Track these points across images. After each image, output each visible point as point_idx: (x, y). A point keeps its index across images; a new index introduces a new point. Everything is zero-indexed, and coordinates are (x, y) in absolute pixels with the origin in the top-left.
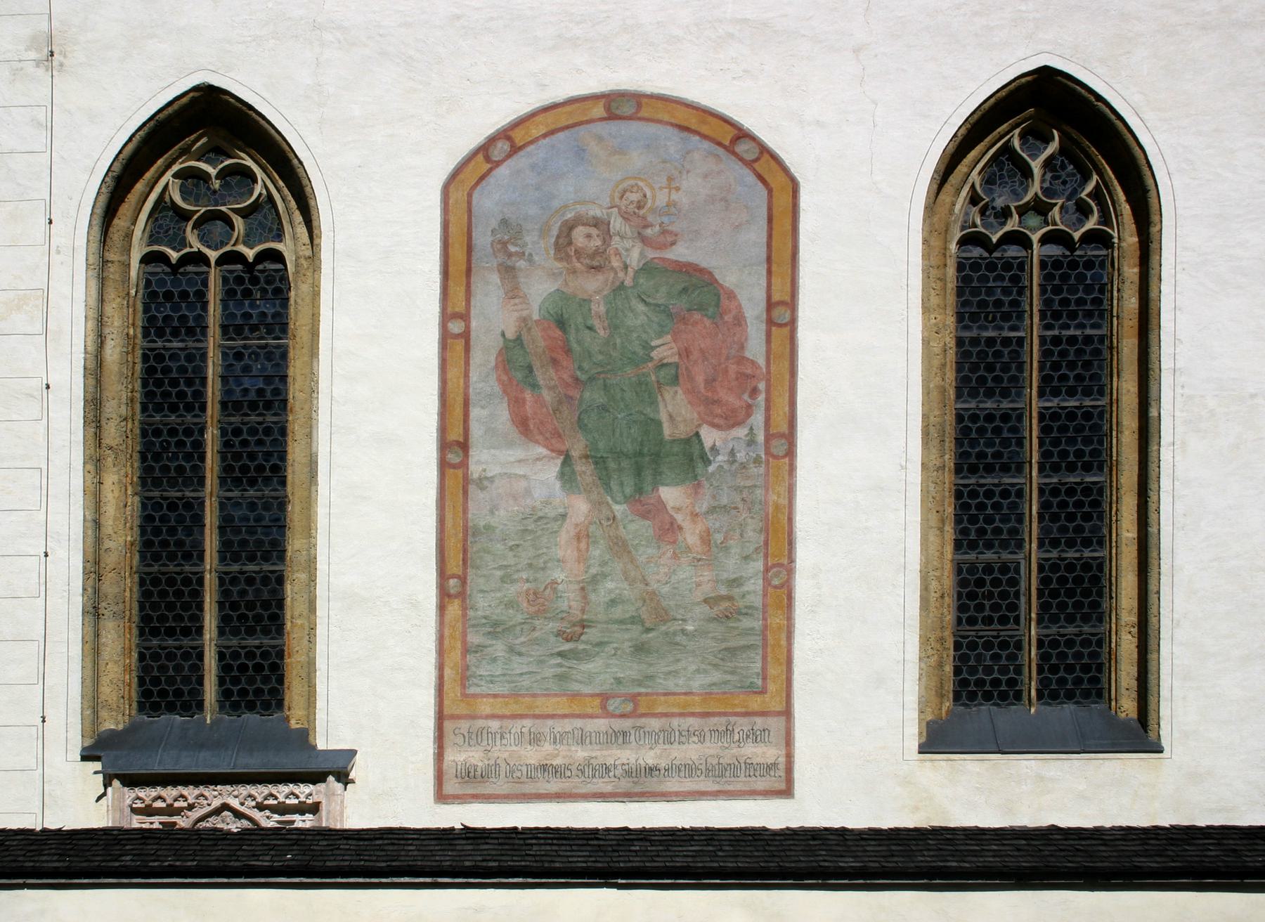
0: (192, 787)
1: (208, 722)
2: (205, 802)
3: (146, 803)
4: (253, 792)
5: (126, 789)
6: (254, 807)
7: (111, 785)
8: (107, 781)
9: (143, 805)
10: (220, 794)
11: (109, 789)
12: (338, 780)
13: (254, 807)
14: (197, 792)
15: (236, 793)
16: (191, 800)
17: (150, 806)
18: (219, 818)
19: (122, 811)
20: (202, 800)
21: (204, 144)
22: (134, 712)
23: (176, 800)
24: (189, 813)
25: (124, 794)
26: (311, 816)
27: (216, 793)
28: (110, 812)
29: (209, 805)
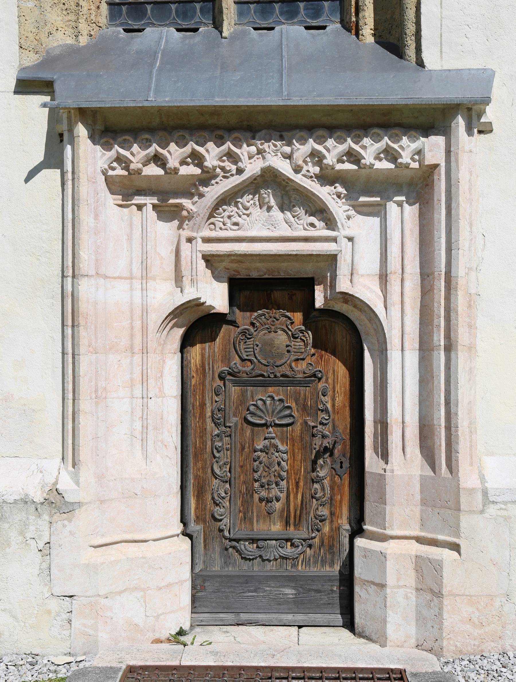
2: (234, 167)
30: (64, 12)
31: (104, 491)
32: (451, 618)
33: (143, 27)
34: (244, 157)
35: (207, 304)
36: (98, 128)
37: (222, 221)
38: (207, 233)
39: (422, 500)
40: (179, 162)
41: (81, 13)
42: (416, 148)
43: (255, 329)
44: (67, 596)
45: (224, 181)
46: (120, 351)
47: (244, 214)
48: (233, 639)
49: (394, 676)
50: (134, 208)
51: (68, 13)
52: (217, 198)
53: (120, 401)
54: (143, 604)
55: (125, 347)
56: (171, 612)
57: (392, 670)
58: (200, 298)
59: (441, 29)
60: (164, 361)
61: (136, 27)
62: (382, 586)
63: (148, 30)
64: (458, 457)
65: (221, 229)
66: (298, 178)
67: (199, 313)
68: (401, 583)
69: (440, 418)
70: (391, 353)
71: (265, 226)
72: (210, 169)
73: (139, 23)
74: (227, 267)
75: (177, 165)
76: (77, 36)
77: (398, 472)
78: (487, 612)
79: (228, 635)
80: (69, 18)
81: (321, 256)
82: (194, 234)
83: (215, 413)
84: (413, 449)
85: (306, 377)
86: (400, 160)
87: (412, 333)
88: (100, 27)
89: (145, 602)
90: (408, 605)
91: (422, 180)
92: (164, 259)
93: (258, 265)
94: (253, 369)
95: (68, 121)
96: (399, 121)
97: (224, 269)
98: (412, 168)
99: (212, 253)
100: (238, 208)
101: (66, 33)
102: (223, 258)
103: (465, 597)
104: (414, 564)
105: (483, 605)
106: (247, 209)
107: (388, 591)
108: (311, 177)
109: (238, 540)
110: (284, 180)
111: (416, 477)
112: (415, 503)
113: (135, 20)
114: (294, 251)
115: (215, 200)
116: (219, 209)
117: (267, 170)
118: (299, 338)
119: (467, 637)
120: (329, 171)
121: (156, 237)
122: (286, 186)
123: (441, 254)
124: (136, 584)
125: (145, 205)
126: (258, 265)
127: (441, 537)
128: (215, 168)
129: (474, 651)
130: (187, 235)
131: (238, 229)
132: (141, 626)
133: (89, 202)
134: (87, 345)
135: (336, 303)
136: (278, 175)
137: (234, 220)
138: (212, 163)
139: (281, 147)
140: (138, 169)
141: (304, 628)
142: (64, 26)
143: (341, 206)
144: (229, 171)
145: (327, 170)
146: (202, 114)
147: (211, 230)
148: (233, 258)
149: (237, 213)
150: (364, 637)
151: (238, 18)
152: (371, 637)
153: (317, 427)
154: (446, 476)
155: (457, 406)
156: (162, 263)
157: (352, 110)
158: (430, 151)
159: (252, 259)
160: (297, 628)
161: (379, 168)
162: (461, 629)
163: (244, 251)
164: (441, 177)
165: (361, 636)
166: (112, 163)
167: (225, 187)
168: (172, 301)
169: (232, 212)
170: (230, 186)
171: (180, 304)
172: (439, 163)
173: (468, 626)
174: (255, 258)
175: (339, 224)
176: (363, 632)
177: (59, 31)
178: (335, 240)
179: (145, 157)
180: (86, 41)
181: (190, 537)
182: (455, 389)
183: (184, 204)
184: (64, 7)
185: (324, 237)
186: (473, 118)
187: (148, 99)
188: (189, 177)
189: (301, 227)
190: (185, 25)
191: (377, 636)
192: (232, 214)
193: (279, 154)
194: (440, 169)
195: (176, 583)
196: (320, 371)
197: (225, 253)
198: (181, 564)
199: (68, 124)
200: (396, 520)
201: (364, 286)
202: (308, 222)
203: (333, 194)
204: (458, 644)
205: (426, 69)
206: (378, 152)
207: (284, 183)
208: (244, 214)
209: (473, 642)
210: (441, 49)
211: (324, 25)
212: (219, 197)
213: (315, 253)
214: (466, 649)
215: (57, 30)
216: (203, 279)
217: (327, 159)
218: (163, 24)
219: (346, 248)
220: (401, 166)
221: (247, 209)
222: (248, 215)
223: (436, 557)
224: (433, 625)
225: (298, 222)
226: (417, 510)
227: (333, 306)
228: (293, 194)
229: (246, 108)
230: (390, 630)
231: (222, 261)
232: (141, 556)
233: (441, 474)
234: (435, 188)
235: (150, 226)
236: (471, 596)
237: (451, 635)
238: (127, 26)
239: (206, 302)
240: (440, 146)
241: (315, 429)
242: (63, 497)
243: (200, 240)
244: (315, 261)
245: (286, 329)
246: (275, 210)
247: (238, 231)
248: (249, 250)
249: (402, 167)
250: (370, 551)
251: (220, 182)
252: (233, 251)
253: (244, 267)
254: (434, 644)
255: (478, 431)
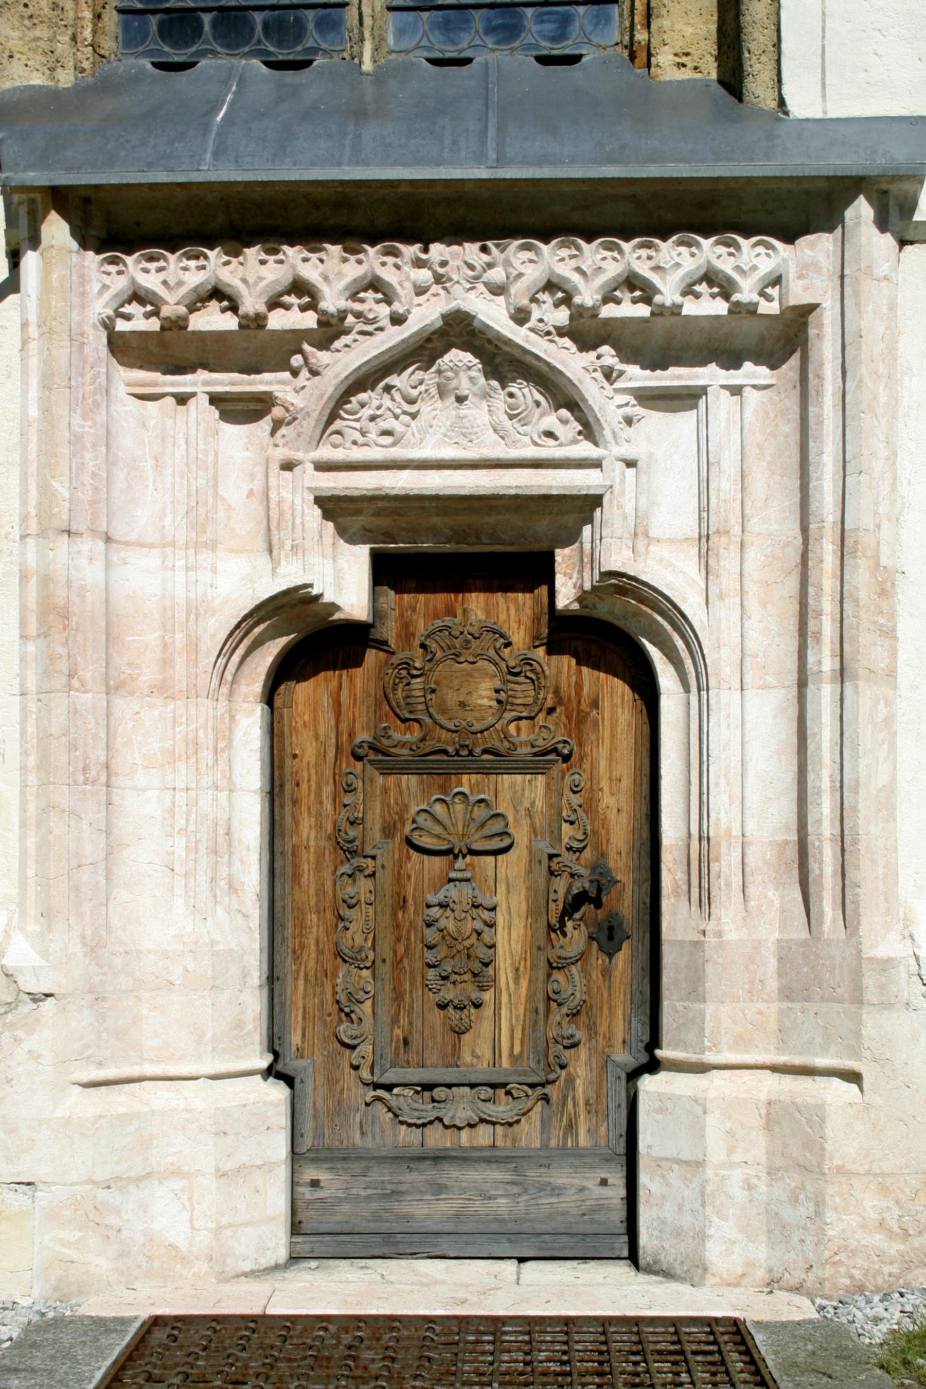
0: (335, 250)
1: (367, 66)
2: (384, 311)
3: (165, 311)
4: (565, 270)
5: (92, 258)
6: (561, 332)
7: (35, 241)
8: (23, 232)
9: (154, 325)
10: (439, 279)
11: (30, 260)
12: (882, 224)
13: (561, 332)
14: (353, 270)
15: (497, 275)
16: (332, 302)
17: (176, 325)
18: (429, 377)
19: (77, 340)
20: (371, 304)
21: (218, 115)
22: (108, 45)
23: (274, 304)
24: (322, 357)
25: (84, 280)
26: (763, 370)
27: (424, 275)
28: (33, 345)
29: (397, 320)
30: (27, 22)
31: (104, 974)
32: (842, 1220)
33: (195, 60)
34: (404, 292)
35: (327, 599)
36: (94, 233)
37: (359, 428)
38: (326, 453)
39: (781, 991)
40: (266, 303)
41: (62, 23)
42: (770, 273)
43: (429, 657)
44: (23, 1183)
45: (362, 343)
46: (138, 694)
47: (405, 413)
48: (378, 1278)
49: (721, 1329)
50: (171, 400)
51: (35, 24)
52: (347, 378)
53: (139, 795)
54: (187, 1203)
55: (150, 686)
56: (246, 1224)
57: (716, 1319)
58: (311, 586)
59: (823, 37)
60: (232, 717)
61: (176, 59)
62: (698, 1164)
63: (203, 63)
64: (857, 895)
65: (355, 443)
66: (520, 335)
67: (308, 619)
68: (737, 1157)
69: (819, 821)
70: (717, 695)
71: (450, 438)
72: (332, 316)
73: (187, 51)
74: (368, 527)
75: (262, 308)
76: (52, 70)
77: (732, 935)
78: (918, 1208)
79: (369, 1271)
80: (38, 33)
81: (569, 500)
82: (299, 455)
83: (342, 828)
84: (763, 889)
85: (535, 755)
86: (735, 297)
87: (761, 654)
88: (102, 56)
89: (190, 1199)
90: (750, 1201)
91: (783, 342)
92: (234, 509)
93: (436, 520)
94: (423, 739)
95: (29, 220)
96: (737, 220)
97: (361, 532)
98: (762, 315)
99: (336, 493)
100: (393, 399)
101: (29, 63)
102: (359, 505)
103: (871, 1178)
104: (764, 1120)
105: (908, 1193)
106: (412, 402)
107: (710, 1173)
108: (548, 333)
109: (389, 1088)
110: (490, 341)
111: (770, 945)
112: (766, 997)
113: (175, 45)
114: (512, 488)
115: (342, 382)
116: (350, 402)
117: (452, 319)
118: (523, 674)
119: (875, 1258)
120: (586, 322)
121: (217, 462)
122: (495, 355)
123: (822, 487)
124: (172, 1164)
125: (194, 394)
126: (436, 520)
127: (821, 1062)
128: (342, 315)
129: (890, 1286)
130: (282, 457)
131: (394, 444)
132: (184, 1250)
133: (73, 383)
134: (67, 673)
135: (600, 598)
136: (477, 331)
137: (384, 425)
138: (336, 304)
139: (485, 271)
140: (178, 317)
141: (529, 1264)
142: (25, 50)
143: (610, 396)
144: (374, 321)
145: (582, 320)
146: (316, 207)
147: (335, 446)
148: (380, 504)
149: (389, 409)
150: (656, 1273)
151: (395, 41)
152: (672, 1272)
153: (558, 855)
154: (832, 937)
155: (856, 792)
156: (229, 518)
157: (634, 196)
158: (799, 278)
159: (422, 508)
160: (515, 1262)
161: (692, 314)
162: (863, 1242)
163: (403, 488)
164: (822, 331)
165: (650, 1270)
166: (122, 306)
167: (364, 355)
168: (250, 591)
169: (378, 408)
170: (376, 352)
171: (266, 596)
172: (819, 302)
173: (878, 1237)
174: (427, 504)
175: (607, 433)
176: (655, 1263)
177: (15, 59)
178: (596, 464)
179: (195, 291)
180: (72, 79)
181: (289, 1081)
182: (852, 757)
183: (277, 394)
184: (27, 12)
185: (575, 460)
186: (891, 211)
187: (201, 168)
188: (288, 335)
189: (527, 439)
190: (282, 55)
191: (685, 1268)
192: (379, 412)
193: (481, 287)
194: (821, 315)
195: (260, 1167)
196: (565, 742)
197: (364, 492)
198: (268, 1129)
199: (29, 226)
200: (726, 1033)
201: (660, 561)
202: (541, 430)
203: (595, 370)
204: (857, 1273)
205: (791, 117)
206: (689, 281)
207: (488, 347)
208: (405, 413)
209: (887, 1269)
210: (823, 79)
211: (577, 52)
212: (351, 374)
213: (555, 493)
214: (873, 1281)
215: (11, 57)
216: (316, 547)
217: (581, 295)
218: (236, 52)
219: (623, 481)
220: (737, 310)
221: (412, 402)
222: (414, 416)
223: (811, 1101)
224: (803, 1237)
225: (520, 429)
226: (773, 1009)
227: (594, 605)
228: (510, 371)
229: (409, 189)
230: (714, 1252)
231: (358, 512)
232: (182, 1107)
233: (823, 933)
234: (810, 353)
235: (205, 439)
236: (883, 1174)
237: (842, 1257)
238: (160, 57)
239: (322, 595)
240: (820, 268)
241: (555, 860)
242: (15, 982)
243: (310, 467)
244: (556, 510)
245: (497, 658)
246: (472, 405)
247: (392, 449)
248: (416, 486)
249: (740, 313)
250: (672, 1097)
251: (353, 345)
252: (380, 489)
253: (404, 525)
254: (804, 1276)
255: (899, 847)
